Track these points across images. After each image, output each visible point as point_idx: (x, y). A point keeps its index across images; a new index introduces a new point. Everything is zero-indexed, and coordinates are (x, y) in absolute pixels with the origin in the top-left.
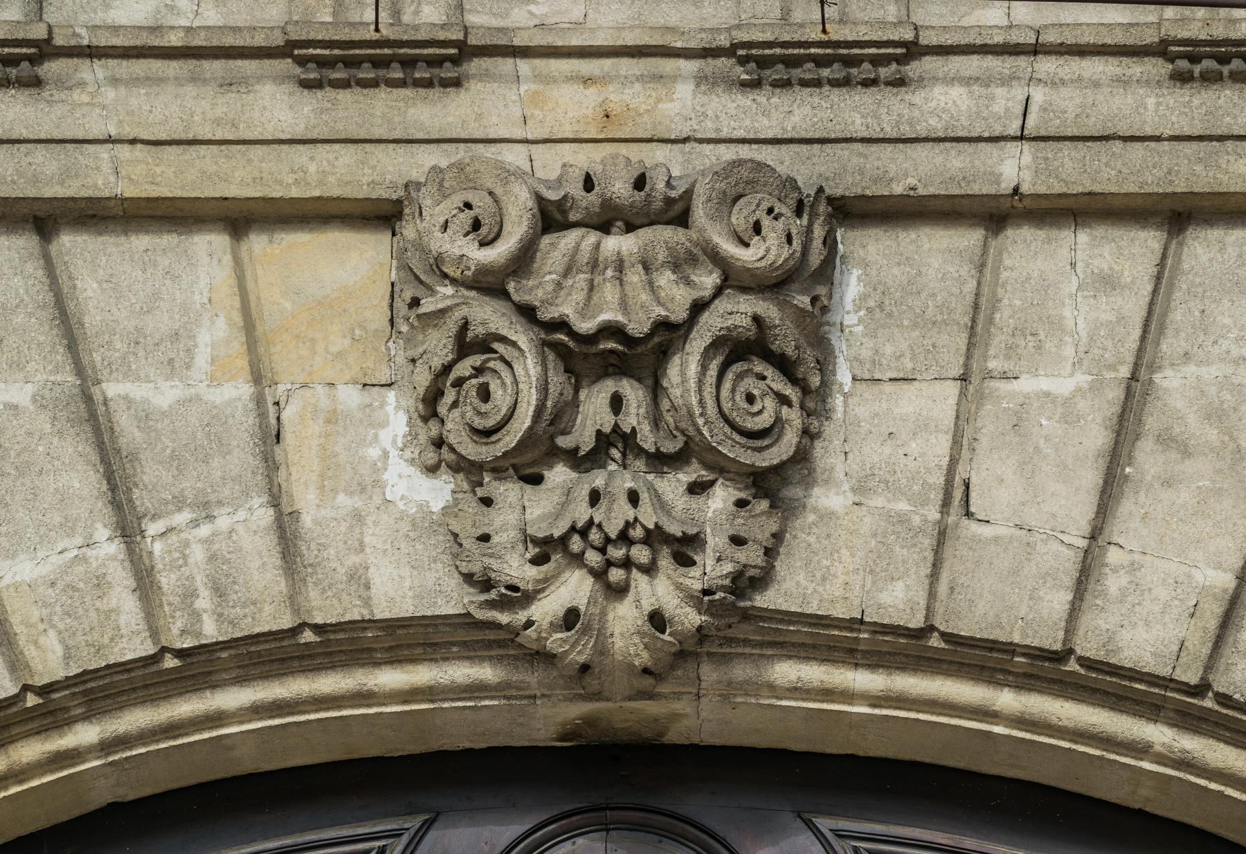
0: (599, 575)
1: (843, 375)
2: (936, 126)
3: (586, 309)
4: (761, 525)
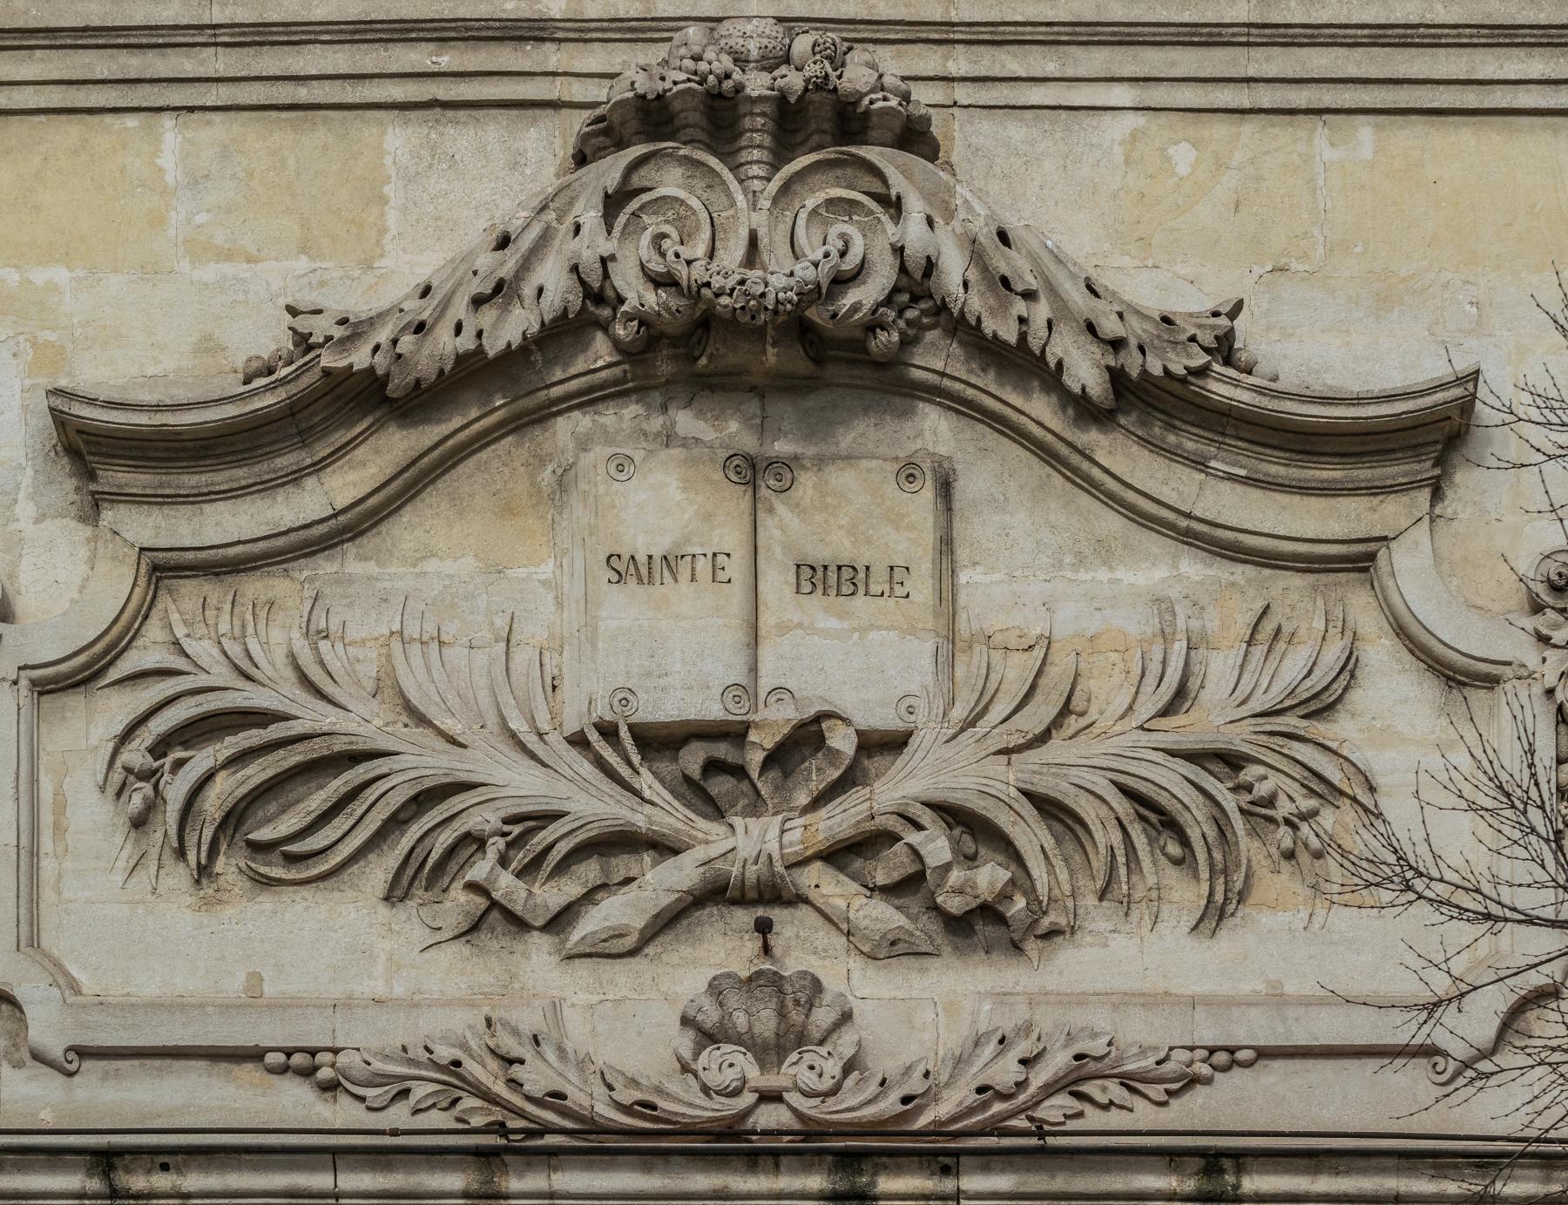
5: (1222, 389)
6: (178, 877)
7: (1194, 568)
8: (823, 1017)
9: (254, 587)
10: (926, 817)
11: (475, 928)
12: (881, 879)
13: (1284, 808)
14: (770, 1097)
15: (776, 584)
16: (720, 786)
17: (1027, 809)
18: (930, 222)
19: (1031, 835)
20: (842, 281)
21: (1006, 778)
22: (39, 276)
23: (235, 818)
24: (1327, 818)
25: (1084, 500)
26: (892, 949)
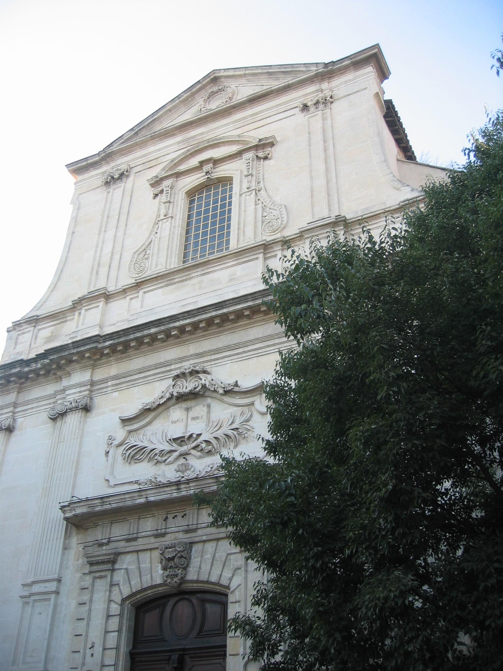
0: (171, 578)
1: (192, 558)
2: (199, 535)
3: (171, 555)
4: (184, 572)
5: (236, 389)
6: (127, 464)
7: (235, 408)
8: (190, 467)
9: (138, 432)
10: (203, 442)
11: (156, 464)
12: (199, 450)
13: (244, 433)
14: (183, 477)
15: (190, 420)
16: (183, 443)
17: (214, 439)
18: (205, 380)
19: (214, 442)
20: (195, 388)
21: (211, 436)
22: (122, 405)
23: (133, 457)
24: (249, 433)
25: (224, 404)
26: (200, 457)
